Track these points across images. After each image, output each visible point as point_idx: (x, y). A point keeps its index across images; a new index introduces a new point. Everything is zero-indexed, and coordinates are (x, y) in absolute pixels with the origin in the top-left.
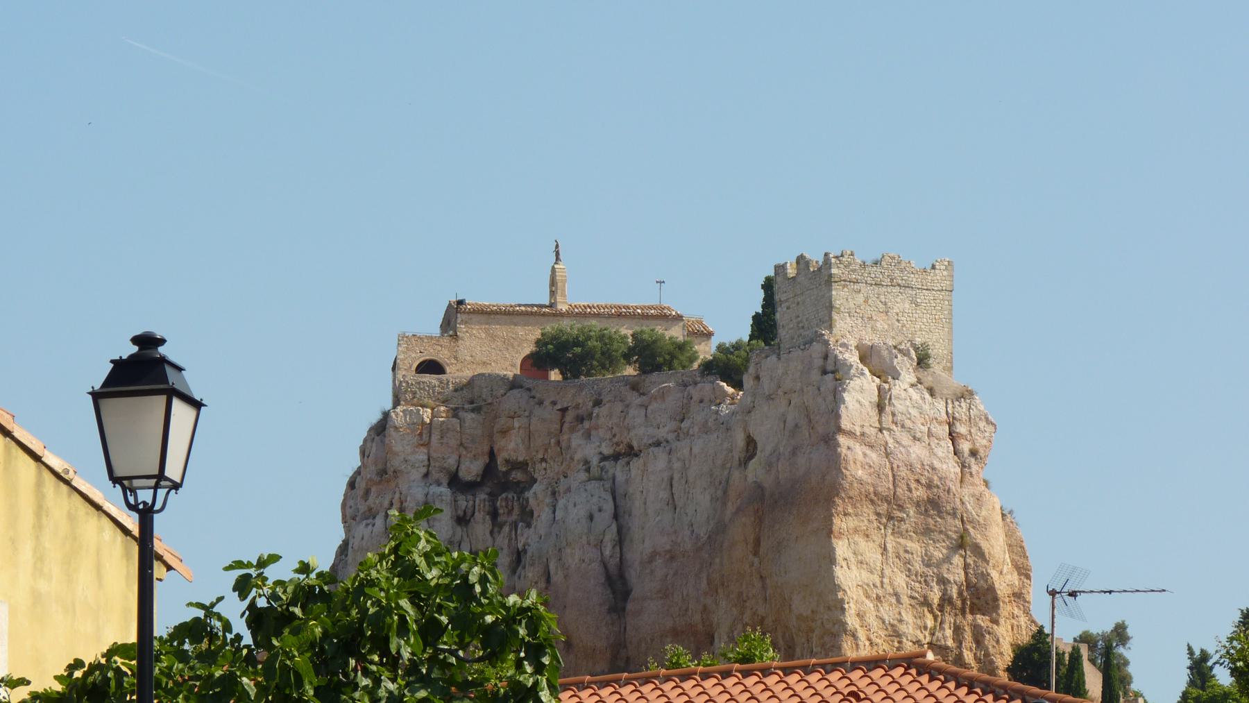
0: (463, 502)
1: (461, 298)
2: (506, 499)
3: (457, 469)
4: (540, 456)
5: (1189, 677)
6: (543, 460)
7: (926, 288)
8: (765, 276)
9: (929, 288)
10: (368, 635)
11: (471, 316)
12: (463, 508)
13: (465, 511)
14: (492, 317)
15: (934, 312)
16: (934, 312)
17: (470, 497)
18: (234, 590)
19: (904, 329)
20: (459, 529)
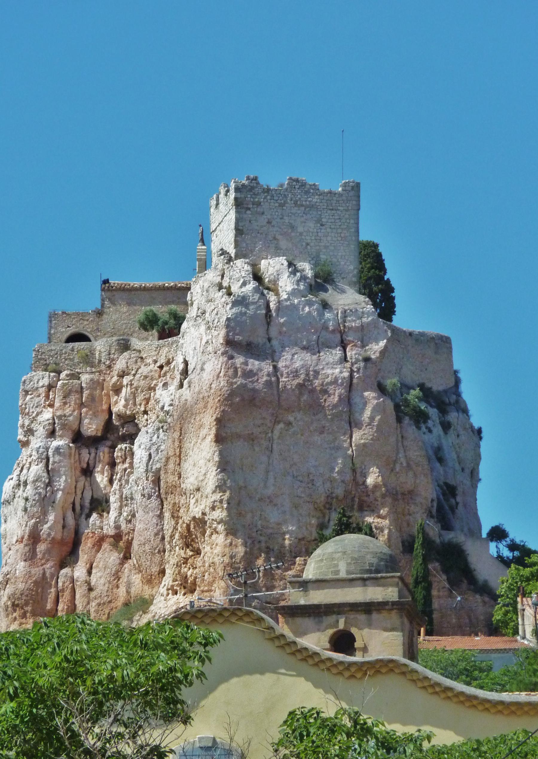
0: (85, 454)
1: (106, 278)
2: (121, 449)
3: (79, 427)
4: (142, 409)
5: (300, 591)
6: (145, 412)
7: (331, 208)
8: (450, 336)
9: (334, 208)
10: (386, 509)
11: (115, 293)
12: (86, 460)
13: (88, 464)
14: (133, 293)
15: (339, 231)
16: (339, 231)
17: (93, 451)
18: (480, 480)
19: (309, 247)
20: (83, 478)
